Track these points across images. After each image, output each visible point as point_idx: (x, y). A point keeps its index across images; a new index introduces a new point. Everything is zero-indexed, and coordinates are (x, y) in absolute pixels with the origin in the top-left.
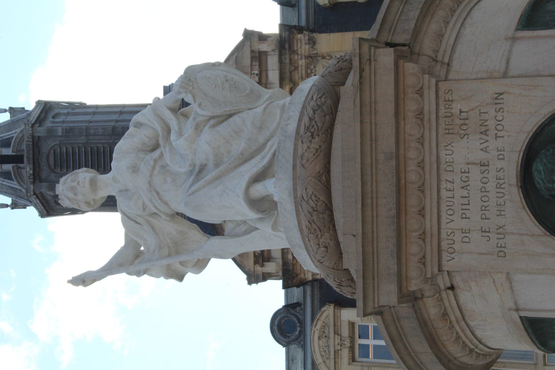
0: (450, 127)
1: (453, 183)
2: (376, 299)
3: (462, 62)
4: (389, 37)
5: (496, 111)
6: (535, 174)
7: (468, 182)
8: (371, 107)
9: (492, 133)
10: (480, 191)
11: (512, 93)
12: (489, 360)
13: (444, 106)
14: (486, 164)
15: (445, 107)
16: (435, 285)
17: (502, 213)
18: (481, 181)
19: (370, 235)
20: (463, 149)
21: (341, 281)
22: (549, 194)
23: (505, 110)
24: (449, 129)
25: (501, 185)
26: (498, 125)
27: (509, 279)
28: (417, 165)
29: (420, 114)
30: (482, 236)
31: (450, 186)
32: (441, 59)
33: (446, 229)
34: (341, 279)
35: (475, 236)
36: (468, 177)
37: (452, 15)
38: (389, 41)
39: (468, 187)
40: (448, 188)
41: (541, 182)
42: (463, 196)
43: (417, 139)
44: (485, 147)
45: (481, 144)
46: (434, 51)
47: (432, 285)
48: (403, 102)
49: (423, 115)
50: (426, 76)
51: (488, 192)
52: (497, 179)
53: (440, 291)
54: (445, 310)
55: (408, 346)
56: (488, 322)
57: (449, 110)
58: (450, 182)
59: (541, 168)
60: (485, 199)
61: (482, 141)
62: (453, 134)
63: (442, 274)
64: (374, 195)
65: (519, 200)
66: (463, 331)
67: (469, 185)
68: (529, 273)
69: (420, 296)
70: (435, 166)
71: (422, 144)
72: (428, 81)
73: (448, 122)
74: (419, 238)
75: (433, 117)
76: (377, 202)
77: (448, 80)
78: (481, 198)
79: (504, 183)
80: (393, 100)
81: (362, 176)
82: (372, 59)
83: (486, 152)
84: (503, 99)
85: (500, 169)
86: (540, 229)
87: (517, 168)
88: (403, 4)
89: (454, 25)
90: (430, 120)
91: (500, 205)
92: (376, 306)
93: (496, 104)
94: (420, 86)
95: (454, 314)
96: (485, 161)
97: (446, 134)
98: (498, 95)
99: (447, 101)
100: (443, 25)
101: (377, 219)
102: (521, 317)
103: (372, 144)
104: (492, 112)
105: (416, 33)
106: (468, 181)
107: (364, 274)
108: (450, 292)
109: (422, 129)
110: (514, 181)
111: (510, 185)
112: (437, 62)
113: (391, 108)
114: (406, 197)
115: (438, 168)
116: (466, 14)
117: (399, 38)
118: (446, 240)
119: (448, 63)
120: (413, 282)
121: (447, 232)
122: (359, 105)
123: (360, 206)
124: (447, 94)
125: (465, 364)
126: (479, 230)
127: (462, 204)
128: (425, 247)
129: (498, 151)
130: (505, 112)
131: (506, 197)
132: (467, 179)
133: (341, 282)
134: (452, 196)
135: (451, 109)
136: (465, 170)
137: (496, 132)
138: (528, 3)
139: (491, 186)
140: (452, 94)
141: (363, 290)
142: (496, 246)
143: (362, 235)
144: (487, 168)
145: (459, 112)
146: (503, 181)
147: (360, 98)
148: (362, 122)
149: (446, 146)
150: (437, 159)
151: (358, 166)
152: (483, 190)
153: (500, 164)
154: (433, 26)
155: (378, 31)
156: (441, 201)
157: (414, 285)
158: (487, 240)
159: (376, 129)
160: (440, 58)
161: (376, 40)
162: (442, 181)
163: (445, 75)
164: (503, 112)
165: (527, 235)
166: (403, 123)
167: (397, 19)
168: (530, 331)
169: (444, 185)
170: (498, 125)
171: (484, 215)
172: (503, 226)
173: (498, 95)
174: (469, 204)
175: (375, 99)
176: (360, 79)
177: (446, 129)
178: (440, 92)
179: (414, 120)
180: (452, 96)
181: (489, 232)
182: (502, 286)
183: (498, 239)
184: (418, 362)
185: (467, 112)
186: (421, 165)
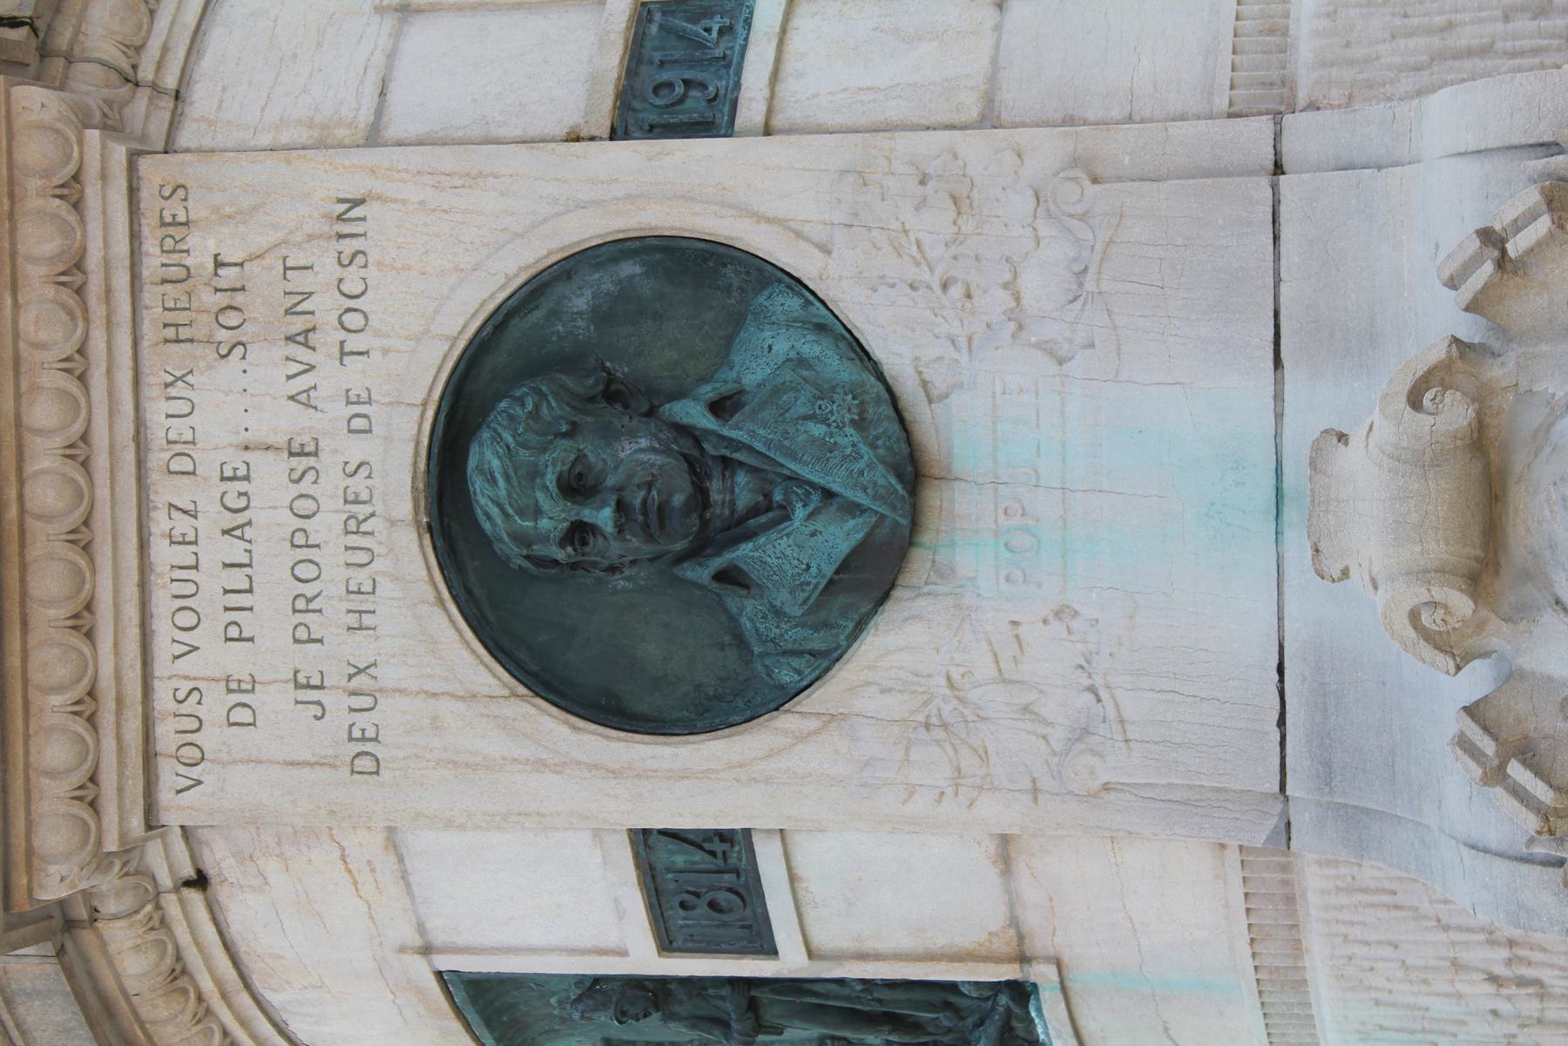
108: (194, 896)
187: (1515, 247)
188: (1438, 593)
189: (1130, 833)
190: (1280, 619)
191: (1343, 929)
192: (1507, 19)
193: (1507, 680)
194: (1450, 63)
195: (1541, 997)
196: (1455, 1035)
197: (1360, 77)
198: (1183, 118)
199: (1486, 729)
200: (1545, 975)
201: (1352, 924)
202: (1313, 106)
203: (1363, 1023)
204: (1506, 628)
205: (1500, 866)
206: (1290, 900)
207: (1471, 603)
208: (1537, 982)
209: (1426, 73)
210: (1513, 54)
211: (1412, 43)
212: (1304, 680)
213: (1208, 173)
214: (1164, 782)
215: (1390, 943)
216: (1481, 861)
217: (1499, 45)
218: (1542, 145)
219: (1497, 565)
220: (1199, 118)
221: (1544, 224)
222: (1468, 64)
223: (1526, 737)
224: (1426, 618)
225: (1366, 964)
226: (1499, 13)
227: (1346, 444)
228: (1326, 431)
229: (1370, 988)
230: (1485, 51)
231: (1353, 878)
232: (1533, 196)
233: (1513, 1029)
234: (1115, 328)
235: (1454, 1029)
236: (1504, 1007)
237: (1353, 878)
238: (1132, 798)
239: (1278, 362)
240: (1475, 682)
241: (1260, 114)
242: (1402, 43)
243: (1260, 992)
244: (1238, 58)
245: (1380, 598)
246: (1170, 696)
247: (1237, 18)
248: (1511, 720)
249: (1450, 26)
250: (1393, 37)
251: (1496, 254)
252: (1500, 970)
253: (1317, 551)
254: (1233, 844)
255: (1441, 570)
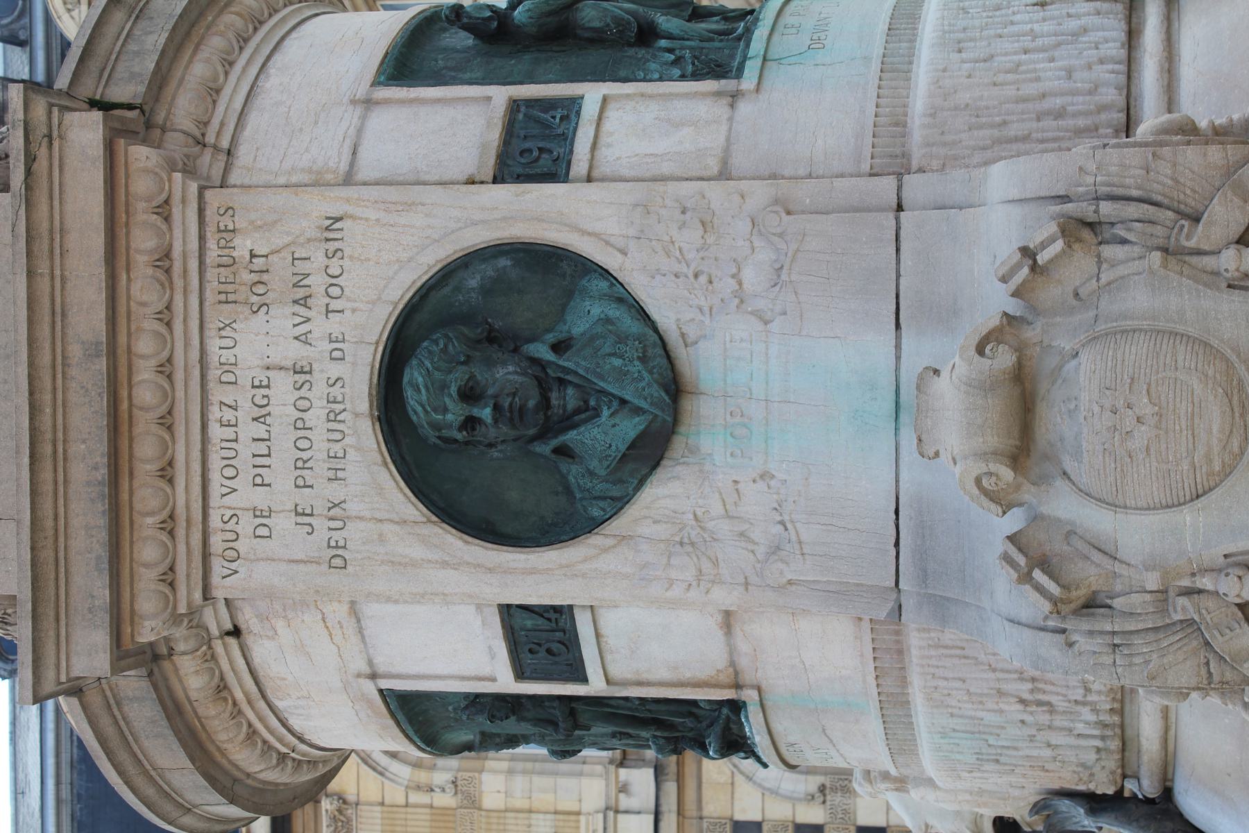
0: (230, 288)
1: (236, 410)
2: (64, 664)
3: (257, 149)
4: (97, 88)
5: (327, 256)
6: (409, 393)
7: (268, 408)
8: (52, 240)
9: (319, 301)
10: (293, 427)
11: (361, 219)
12: (322, 770)
13: (215, 242)
14: (305, 370)
15: (218, 244)
16: (198, 626)
17: (340, 474)
18: (295, 406)
19: (49, 523)
20: (257, 335)
21: (5, 614)
22: (437, 434)
23: (346, 255)
24: (227, 293)
25: (336, 415)
26: (332, 285)
27: (355, 613)
28: (155, 369)
29: (163, 260)
30: (297, 524)
31: (228, 415)
32: (213, 141)
33: (219, 508)
34: (5, 610)
35: (283, 523)
36: (267, 396)
37: (241, 48)
38: (98, 97)
39: (268, 417)
40: (224, 419)
41: (419, 409)
42: (256, 437)
43: (156, 313)
44: (305, 332)
45: (295, 326)
46: (199, 122)
47: (191, 627)
48: (124, 230)
49: (171, 260)
50: (178, 176)
51: (311, 429)
52: (328, 402)
53: (210, 640)
54: (222, 678)
55: (141, 757)
56: (314, 701)
57: (226, 251)
58: (230, 407)
59: (420, 380)
60: (303, 444)
61: (298, 320)
62: (235, 302)
63: (214, 604)
64: (60, 435)
65: (376, 446)
66: (261, 719)
67: (269, 414)
68: (396, 602)
69: (165, 651)
70: (196, 373)
71: (169, 324)
72: (182, 187)
73: (226, 277)
74: (161, 529)
75: (193, 265)
76: (65, 451)
77: (227, 187)
78: (295, 442)
79: (344, 410)
80: (103, 226)
81: (31, 393)
82: (55, 134)
83: (306, 343)
84: (342, 230)
85: (336, 381)
86: (417, 509)
87: (371, 379)
88: (134, 16)
89: (244, 70)
90: (185, 271)
91: (336, 457)
92: (63, 678)
93: (327, 240)
94: (164, 196)
95: (241, 687)
96: (304, 363)
97: (220, 302)
98: (331, 221)
99: (223, 231)
100: (220, 68)
101: (65, 487)
102: (381, 691)
103: (54, 322)
104: (319, 259)
105: (160, 80)
106: (268, 405)
107: (34, 610)
108: (232, 641)
109: (168, 292)
110: (364, 405)
111: (357, 415)
112: (205, 146)
113: (98, 242)
114: (131, 439)
115: (203, 377)
116: (271, 47)
117: (121, 92)
118: (220, 532)
119: (229, 150)
120: (147, 623)
121: (223, 515)
122: (25, 235)
123: (26, 460)
124: (224, 217)
125: (270, 783)
126: (291, 511)
127: (254, 456)
128: (175, 546)
129: (331, 341)
130: (345, 259)
131: (347, 440)
132: (265, 402)
133: (6, 616)
134: (233, 437)
135: (232, 250)
136: (261, 381)
137: (327, 300)
138: (401, 29)
139: (316, 417)
140: (233, 216)
141: (34, 645)
142: (326, 545)
143: (32, 523)
144: (308, 377)
145: (248, 257)
146: (341, 407)
147: (27, 219)
148: (31, 274)
149: (220, 329)
150: (202, 358)
151: (23, 370)
152: (300, 425)
153: (335, 370)
154: (199, 69)
155: (74, 74)
156: (210, 447)
157: (148, 633)
158: (308, 533)
159: (63, 288)
160: (210, 138)
161: (67, 93)
162: (212, 404)
163: (221, 174)
164: (342, 258)
165: (392, 521)
166: (124, 277)
167: (117, 49)
168: (400, 717)
169: (215, 413)
170: (332, 285)
171: (300, 479)
172: (340, 503)
173: (331, 221)
174: (269, 455)
175: (61, 223)
176: (26, 179)
177: (220, 293)
178: (208, 212)
179: (150, 271)
180: (233, 221)
181: (311, 515)
182: (341, 627)
183: (330, 529)
184: (166, 787)
185: (267, 256)
186: (165, 369)
187: (1042, 258)
188: (993, 467)
189: (804, 610)
190: (897, 481)
191: (932, 670)
192: (1038, 119)
193: (1033, 521)
194: (1004, 146)
195: (1051, 712)
196: (998, 735)
197: (949, 153)
198: (842, 176)
199: (1020, 550)
200: (1054, 699)
201: (938, 667)
202: (921, 170)
203: (943, 728)
204: (1033, 489)
205: (1027, 633)
206: (900, 652)
207: (1012, 473)
208: (1049, 704)
209: (988, 151)
210: (1042, 141)
211: (981, 133)
212: (911, 518)
213: (857, 210)
214: (825, 580)
215: (960, 679)
216: (1015, 630)
217: (1034, 135)
218: (1059, 197)
219: (1029, 450)
220: (852, 176)
221: (1059, 245)
222: (1015, 147)
223: (1044, 555)
224: (985, 482)
225: (946, 692)
226: (1034, 116)
227: (939, 376)
228: (926, 368)
229: (948, 706)
230: (1025, 139)
231: (939, 639)
232: (1053, 228)
233: (1034, 732)
234: (799, 303)
235: (998, 731)
236: (1029, 719)
237: (939, 639)
238: (806, 589)
239: (898, 326)
240: (1013, 521)
241: (889, 174)
242: (976, 133)
243: (881, 708)
244: (876, 140)
245: (958, 470)
246: (829, 528)
247: (876, 116)
248: (1035, 545)
249: (1005, 123)
250: (970, 129)
251: (1031, 262)
252: (1026, 696)
253: (920, 440)
254: (867, 618)
255: (995, 453)
